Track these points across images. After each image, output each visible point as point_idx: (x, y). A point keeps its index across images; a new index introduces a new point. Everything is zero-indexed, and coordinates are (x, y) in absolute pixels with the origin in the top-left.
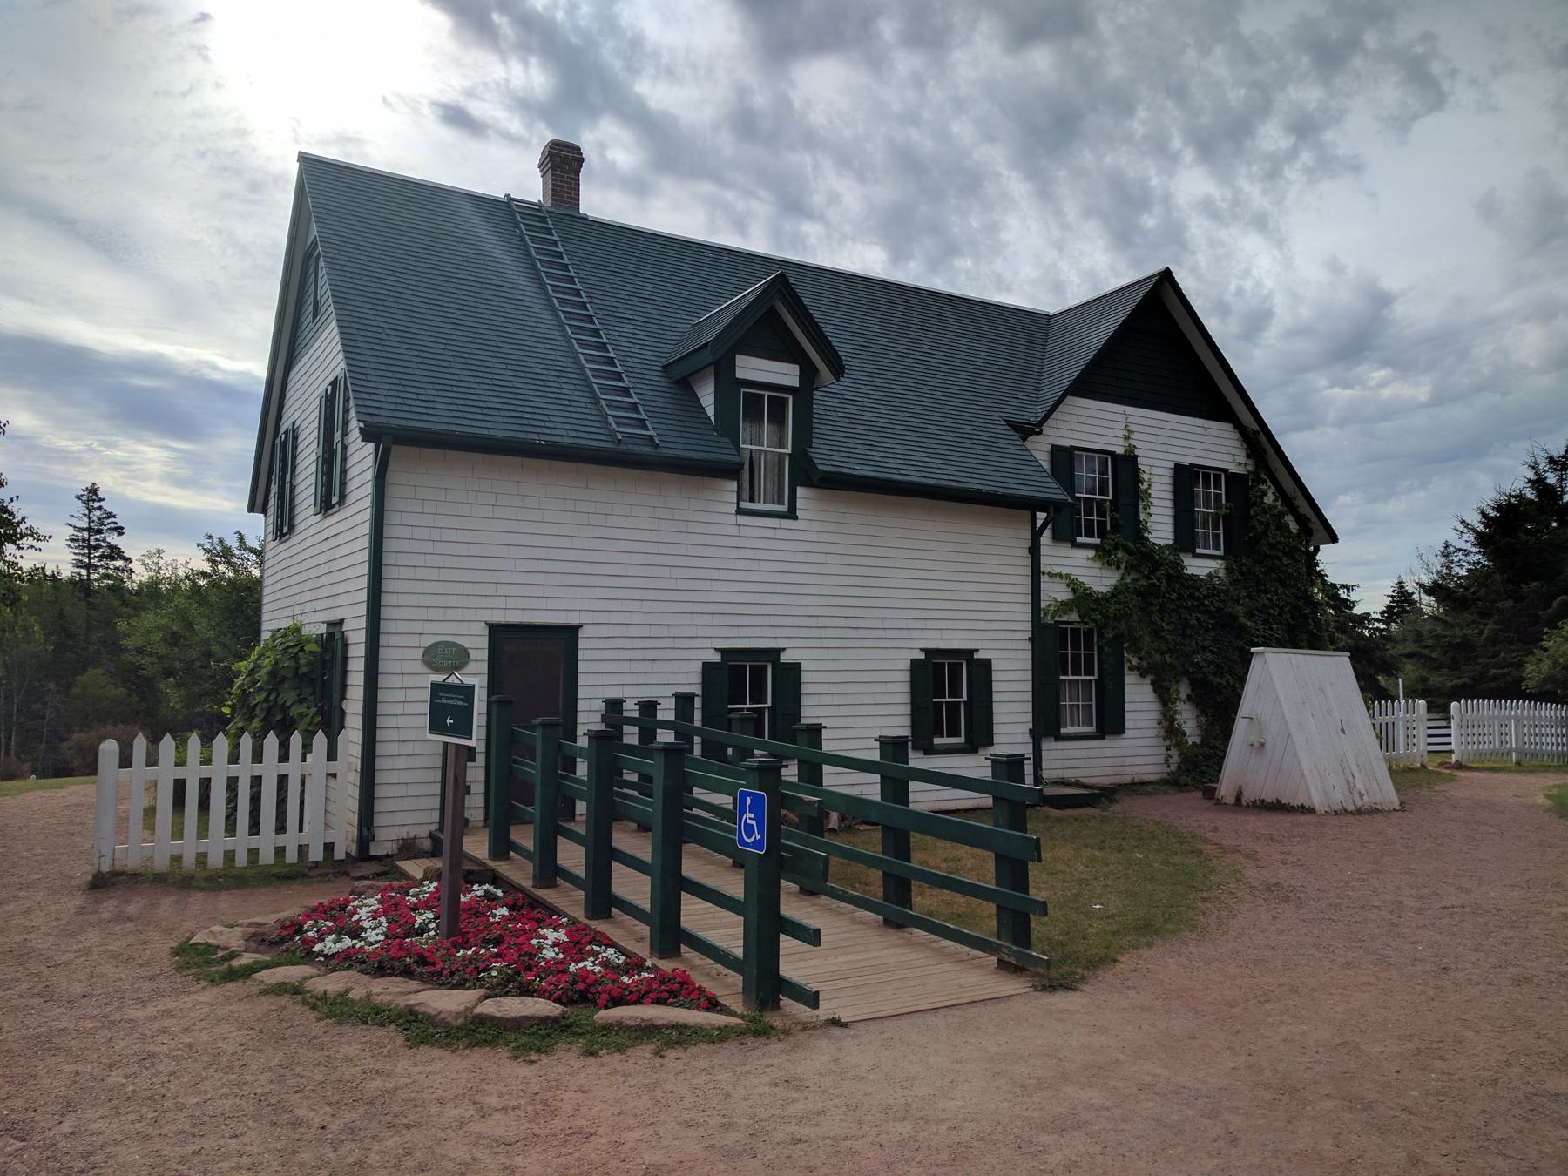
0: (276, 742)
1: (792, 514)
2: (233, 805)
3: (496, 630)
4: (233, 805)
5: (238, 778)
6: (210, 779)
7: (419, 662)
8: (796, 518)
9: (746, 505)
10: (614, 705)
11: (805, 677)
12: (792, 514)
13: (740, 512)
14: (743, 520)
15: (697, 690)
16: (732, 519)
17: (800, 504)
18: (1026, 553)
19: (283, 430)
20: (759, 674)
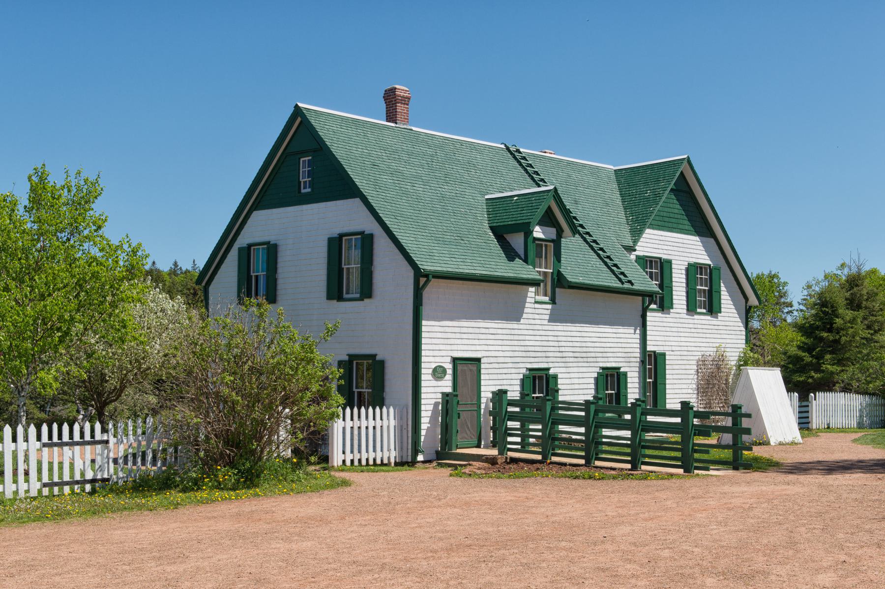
14: (537, 306)
19: (243, 240)
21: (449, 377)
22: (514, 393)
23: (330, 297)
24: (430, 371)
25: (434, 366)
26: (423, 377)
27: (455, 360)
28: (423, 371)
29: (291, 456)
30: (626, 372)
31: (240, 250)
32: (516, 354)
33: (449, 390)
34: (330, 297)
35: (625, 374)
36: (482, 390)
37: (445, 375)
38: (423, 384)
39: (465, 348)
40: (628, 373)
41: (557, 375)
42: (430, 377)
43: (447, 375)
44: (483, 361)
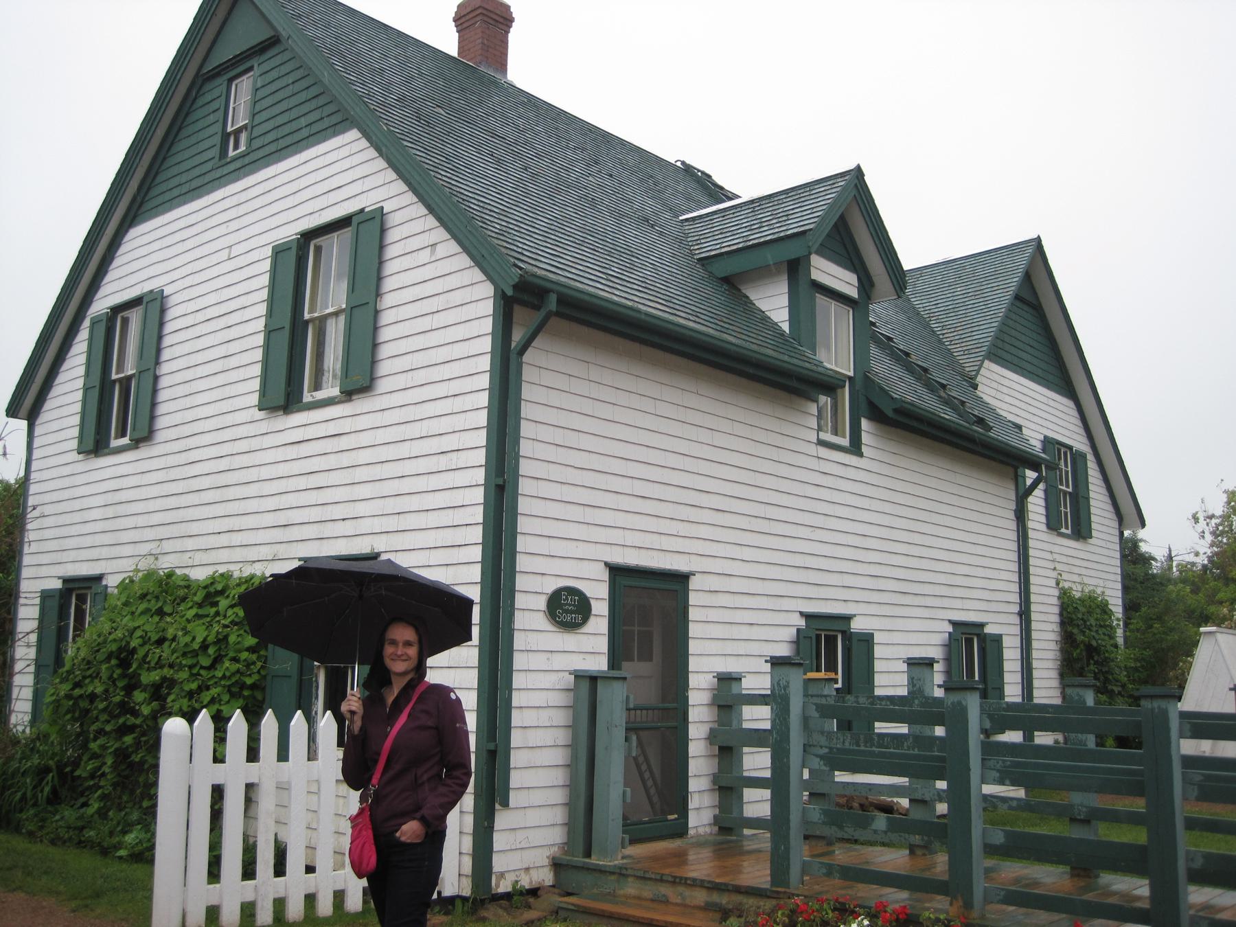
0: (210, 726)
1: (855, 448)
2: (216, 807)
3: (617, 572)
4: (216, 807)
5: (278, 761)
6: (309, 760)
7: (541, 615)
8: (861, 455)
9: (827, 437)
10: (727, 680)
11: (878, 651)
12: (855, 448)
13: (821, 443)
14: (824, 452)
15: (936, 653)
16: (813, 449)
17: (865, 438)
18: (1012, 515)
19: (102, 304)
20: (831, 641)
21: (599, 624)
22: (758, 681)
23: (279, 760)
24: (541, 603)
25: (551, 586)
26: (520, 620)
27: (617, 572)
28: (520, 601)
29: (147, 686)
30: (1001, 636)
31: (94, 323)
32: (77, 517)
33: (600, 664)
34: (279, 760)
35: (998, 639)
36: (690, 669)
37: (586, 619)
38: (519, 641)
39: (647, 540)
40: (1004, 638)
41: (873, 634)
42: (542, 622)
43: (592, 620)
44: (694, 583)
